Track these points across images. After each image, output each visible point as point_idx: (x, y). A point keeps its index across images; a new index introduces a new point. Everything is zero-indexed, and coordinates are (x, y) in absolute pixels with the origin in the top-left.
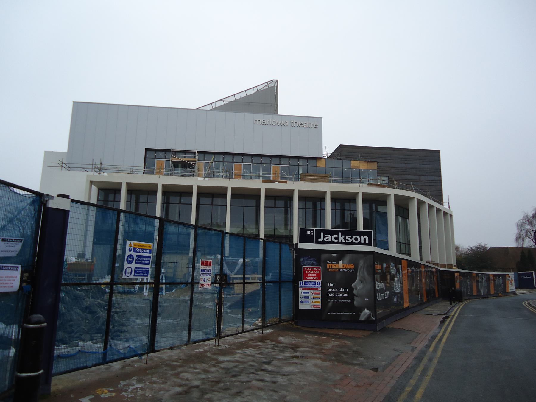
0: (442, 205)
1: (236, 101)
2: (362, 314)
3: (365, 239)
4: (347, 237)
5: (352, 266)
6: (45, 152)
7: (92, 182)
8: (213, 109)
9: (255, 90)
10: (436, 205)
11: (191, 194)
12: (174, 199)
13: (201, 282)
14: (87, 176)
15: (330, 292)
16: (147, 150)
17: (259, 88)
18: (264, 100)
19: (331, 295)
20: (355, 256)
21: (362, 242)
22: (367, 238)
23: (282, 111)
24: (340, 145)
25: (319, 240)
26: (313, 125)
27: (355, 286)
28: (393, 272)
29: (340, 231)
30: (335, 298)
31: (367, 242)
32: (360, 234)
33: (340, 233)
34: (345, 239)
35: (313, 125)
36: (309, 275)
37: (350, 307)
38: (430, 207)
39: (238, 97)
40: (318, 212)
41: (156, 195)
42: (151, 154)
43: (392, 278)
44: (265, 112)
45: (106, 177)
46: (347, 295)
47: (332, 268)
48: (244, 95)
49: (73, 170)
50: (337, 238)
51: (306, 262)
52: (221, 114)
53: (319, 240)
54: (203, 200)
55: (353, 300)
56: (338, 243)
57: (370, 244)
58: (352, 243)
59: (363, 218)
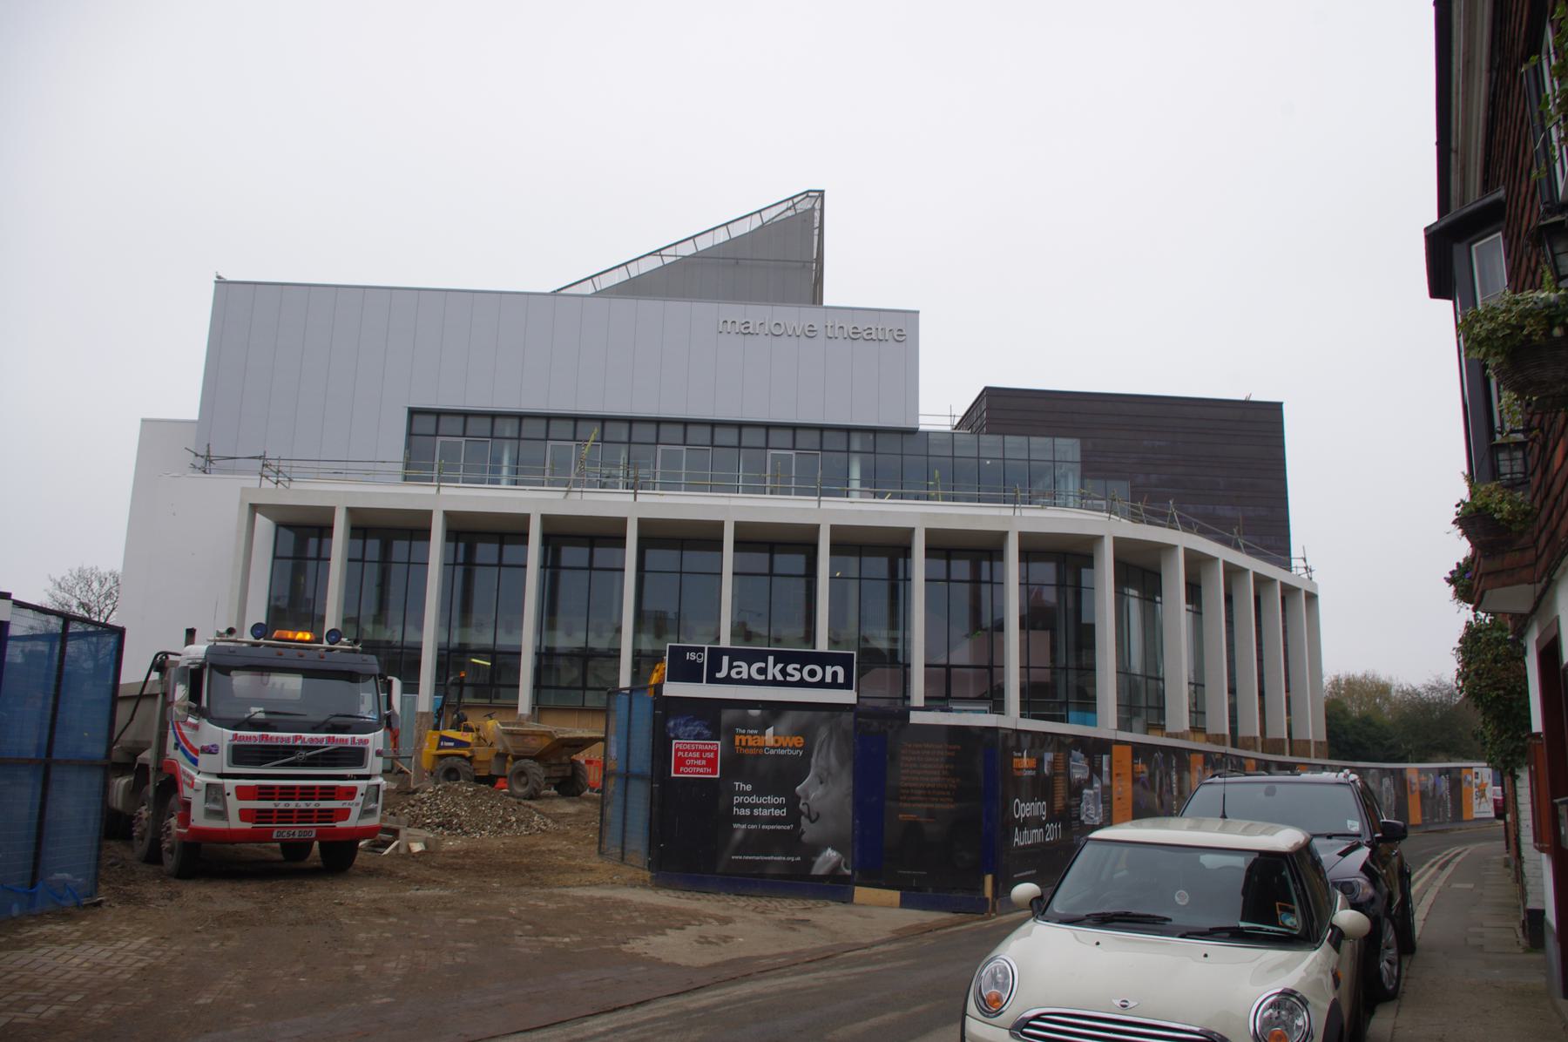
0: (1287, 566)
1: (699, 257)
2: (820, 860)
3: (835, 674)
4: (790, 669)
5: (798, 741)
6: (143, 421)
7: (254, 508)
8: (597, 294)
9: (756, 222)
11: (620, 541)
12: (572, 555)
14: (243, 489)
15: (740, 805)
16: (413, 412)
17: (767, 216)
18: (778, 256)
19: (746, 812)
20: (807, 715)
21: (828, 679)
22: (840, 670)
23: (830, 298)
24: (986, 389)
25: (718, 675)
26: (893, 334)
30: (752, 819)
31: (841, 679)
32: (823, 660)
33: (771, 659)
34: (783, 672)
35: (893, 334)
37: (790, 841)
38: (1262, 582)
39: (704, 243)
42: (427, 424)
43: (1076, 791)
44: (783, 297)
45: (309, 492)
46: (783, 812)
48: (721, 236)
49: (222, 471)
50: (762, 671)
51: (681, 730)
52: (625, 305)
53: (718, 675)
54: (656, 557)
55: (798, 824)
56: (765, 683)
57: (847, 685)
58: (802, 684)
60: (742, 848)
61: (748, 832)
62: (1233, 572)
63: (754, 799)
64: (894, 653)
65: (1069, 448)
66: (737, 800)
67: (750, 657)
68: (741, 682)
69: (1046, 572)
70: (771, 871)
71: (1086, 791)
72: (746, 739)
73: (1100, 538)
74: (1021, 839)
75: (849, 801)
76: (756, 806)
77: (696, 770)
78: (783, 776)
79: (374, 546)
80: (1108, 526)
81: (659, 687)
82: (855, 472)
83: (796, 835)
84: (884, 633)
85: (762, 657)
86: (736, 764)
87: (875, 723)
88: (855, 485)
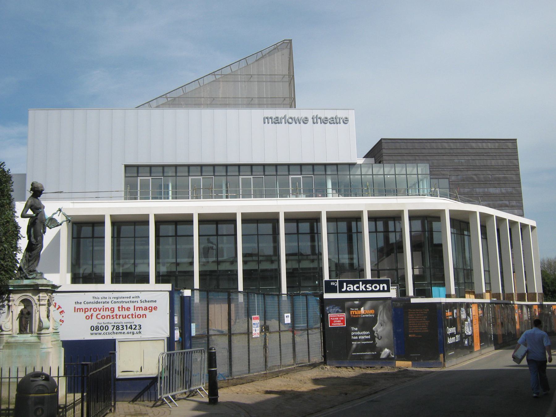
0: (513, 201)
2: (383, 353)
3: (383, 287)
4: (368, 286)
5: (372, 311)
10: (508, 216)
13: (254, 332)
15: (354, 335)
16: (126, 166)
19: (355, 338)
20: (375, 302)
21: (381, 289)
22: (385, 286)
27: (376, 329)
28: (463, 316)
29: (361, 281)
30: (358, 340)
31: (386, 289)
33: (361, 283)
34: (365, 287)
36: (335, 321)
37: (372, 347)
40: (354, 236)
41: (149, 225)
43: (463, 324)
46: (369, 337)
47: (355, 314)
50: (358, 287)
51: (331, 310)
55: (374, 341)
56: (359, 292)
58: (372, 291)
59: (450, 219)
60: (356, 350)
61: (357, 344)
62: (500, 220)
63: (359, 333)
64: (351, 265)
65: (423, 169)
66: (353, 333)
67: (353, 283)
68: (351, 292)
69: (418, 224)
70: (366, 358)
71: (466, 322)
72: (353, 312)
73: (444, 211)
74: (451, 341)
75: (392, 331)
76: (359, 335)
77: (338, 324)
78: (368, 324)
79: (380, 225)
80: (447, 205)
81: (322, 295)
82: (329, 185)
83: (374, 345)
84: (346, 256)
85: (358, 282)
86: (352, 321)
87: (399, 304)
88: (330, 191)
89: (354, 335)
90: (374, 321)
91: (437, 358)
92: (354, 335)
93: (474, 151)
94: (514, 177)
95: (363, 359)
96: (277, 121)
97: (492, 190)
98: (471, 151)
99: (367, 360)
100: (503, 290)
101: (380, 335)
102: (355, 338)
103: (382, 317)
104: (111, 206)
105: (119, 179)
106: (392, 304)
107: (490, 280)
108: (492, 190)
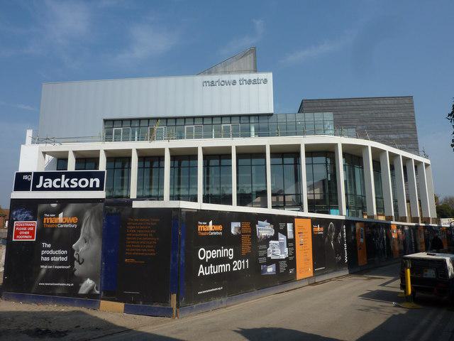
2: (83, 286)
3: (95, 183)
4: (72, 181)
5: (75, 220)
21: (91, 186)
22: (97, 180)
27: (76, 247)
30: (50, 263)
31: (98, 186)
33: (63, 176)
34: (69, 183)
37: (68, 275)
46: (65, 259)
50: (59, 183)
51: (19, 216)
55: (73, 265)
58: (78, 189)
62: (393, 156)
63: (52, 252)
65: (329, 116)
66: (43, 252)
68: (48, 189)
70: (59, 291)
72: (49, 219)
75: (100, 254)
76: (53, 256)
77: (25, 238)
78: (66, 239)
80: (340, 141)
82: (253, 129)
83: (72, 270)
89: (45, 255)
90: (75, 234)
91: (166, 300)
92: (45, 255)
93: (377, 106)
94: (411, 126)
95: (53, 294)
96: (212, 84)
97: (392, 136)
98: (374, 106)
99: (59, 294)
100: (421, 215)
101: (82, 256)
102: (47, 259)
103: (89, 228)
104: (102, 147)
105: (100, 128)
106: (105, 210)
107: (364, 193)
108: (392, 136)
